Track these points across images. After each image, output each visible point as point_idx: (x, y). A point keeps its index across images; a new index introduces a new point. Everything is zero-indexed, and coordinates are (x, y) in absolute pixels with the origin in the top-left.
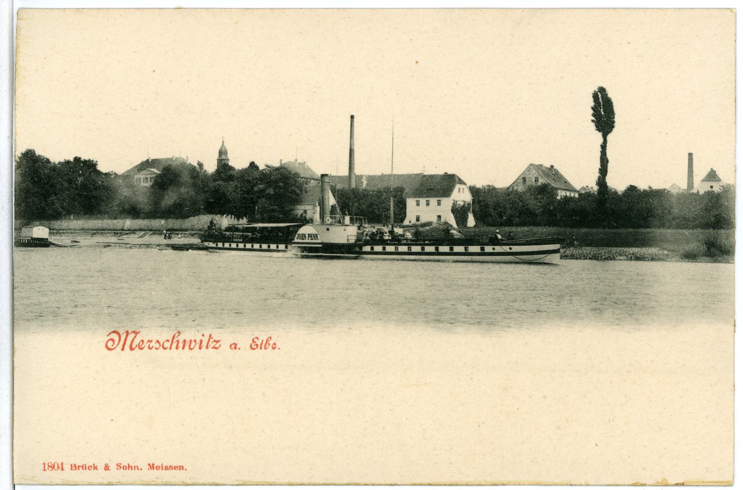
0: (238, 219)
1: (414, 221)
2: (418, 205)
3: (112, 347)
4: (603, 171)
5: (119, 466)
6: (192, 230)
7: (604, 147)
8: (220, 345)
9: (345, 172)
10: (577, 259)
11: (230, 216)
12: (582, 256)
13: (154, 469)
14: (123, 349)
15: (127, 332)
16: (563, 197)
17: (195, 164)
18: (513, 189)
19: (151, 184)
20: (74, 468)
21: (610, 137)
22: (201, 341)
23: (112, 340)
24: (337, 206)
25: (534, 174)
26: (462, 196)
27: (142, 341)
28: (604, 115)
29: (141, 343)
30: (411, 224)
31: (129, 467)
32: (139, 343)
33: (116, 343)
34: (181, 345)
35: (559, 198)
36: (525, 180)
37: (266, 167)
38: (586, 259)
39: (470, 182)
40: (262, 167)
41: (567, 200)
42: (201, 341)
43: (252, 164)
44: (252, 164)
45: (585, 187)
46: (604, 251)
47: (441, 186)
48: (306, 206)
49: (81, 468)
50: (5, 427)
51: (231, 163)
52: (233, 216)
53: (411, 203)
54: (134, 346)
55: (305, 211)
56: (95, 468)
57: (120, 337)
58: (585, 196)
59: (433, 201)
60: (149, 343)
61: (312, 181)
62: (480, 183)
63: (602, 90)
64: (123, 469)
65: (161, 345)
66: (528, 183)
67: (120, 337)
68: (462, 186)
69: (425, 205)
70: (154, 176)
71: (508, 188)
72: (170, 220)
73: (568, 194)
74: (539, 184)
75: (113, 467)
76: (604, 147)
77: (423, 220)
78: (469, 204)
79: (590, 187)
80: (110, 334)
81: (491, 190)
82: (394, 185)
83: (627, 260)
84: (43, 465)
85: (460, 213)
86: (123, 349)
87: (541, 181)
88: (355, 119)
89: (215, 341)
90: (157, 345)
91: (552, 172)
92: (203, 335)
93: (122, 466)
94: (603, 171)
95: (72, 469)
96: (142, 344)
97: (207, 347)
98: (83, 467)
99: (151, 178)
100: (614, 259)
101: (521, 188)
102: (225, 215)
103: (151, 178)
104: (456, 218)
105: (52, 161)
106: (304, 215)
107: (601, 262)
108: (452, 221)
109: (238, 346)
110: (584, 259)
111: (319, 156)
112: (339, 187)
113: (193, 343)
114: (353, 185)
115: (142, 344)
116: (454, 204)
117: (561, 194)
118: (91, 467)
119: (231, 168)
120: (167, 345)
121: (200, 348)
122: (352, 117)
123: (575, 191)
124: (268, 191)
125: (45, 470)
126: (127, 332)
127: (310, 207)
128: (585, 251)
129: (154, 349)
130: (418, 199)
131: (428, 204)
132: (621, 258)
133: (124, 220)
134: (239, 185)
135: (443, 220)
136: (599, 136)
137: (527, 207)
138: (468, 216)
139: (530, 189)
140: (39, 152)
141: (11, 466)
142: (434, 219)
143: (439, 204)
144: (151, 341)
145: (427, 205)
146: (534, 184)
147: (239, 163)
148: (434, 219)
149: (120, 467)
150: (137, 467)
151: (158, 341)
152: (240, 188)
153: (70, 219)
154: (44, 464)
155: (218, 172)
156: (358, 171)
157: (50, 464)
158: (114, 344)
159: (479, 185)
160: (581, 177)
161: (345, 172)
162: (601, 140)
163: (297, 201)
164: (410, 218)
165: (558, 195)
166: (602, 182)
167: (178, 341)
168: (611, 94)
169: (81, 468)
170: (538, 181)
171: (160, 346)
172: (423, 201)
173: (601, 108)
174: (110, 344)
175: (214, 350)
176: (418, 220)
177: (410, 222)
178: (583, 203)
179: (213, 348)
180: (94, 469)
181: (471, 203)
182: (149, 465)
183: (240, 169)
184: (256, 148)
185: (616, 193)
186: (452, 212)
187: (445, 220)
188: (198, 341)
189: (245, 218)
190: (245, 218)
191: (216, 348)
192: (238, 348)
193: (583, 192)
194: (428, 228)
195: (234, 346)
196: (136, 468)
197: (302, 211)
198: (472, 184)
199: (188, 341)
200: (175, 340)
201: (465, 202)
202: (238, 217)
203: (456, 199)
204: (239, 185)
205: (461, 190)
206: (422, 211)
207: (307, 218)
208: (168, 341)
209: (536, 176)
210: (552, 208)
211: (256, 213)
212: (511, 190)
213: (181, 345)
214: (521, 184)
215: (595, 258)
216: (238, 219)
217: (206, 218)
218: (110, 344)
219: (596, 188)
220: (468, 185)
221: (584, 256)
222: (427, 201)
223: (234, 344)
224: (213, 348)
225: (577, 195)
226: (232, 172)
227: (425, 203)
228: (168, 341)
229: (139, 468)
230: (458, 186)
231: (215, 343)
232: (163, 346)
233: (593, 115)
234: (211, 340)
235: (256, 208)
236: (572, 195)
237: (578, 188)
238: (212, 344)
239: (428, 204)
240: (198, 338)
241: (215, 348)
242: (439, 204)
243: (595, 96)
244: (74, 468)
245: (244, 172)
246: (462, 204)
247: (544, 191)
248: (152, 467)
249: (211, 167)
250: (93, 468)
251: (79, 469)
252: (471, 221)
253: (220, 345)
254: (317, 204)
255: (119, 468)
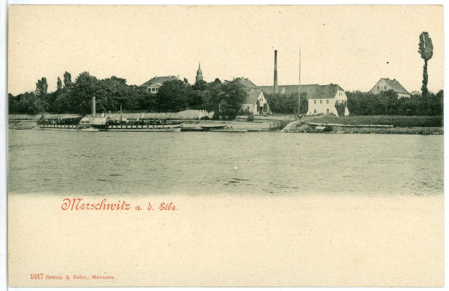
0: (209, 112)
1: (313, 113)
2: (315, 103)
3: (66, 208)
4: (425, 82)
5: (75, 277)
6: (181, 119)
7: (425, 68)
8: (130, 207)
9: (271, 83)
10: (410, 134)
11: (204, 110)
12: (413, 132)
13: (95, 278)
14: (72, 209)
15: (74, 199)
16: (401, 98)
17: (183, 80)
18: (371, 93)
19: (157, 92)
20: (48, 278)
21: (429, 62)
22: (118, 205)
23: (66, 204)
24: (267, 104)
25: (383, 84)
26: (341, 98)
27: (84, 205)
28: (426, 48)
29: (83, 206)
30: (311, 115)
31: (81, 277)
32: (81, 206)
33: (67, 207)
34: (106, 207)
35: (399, 98)
36: (379, 88)
37: (225, 81)
38: (415, 134)
39: (346, 89)
40: (223, 81)
41: (403, 99)
42: (118, 205)
43: (217, 80)
44: (217, 80)
45: (414, 91)
46: (425, 129)
47: (333, 89)
48: (249, 104)
49: (52, 278)
50: (3, 255)
51: (204, 79)
52: (206, 111)
53: (311, 102)
54: (78, 208)
55: (249, 108)
56: (61, 278)
57: (70, 201)
58: (415, 97)
59: (324, 100)
60: (87, 206)
61: (252, 89)
62: (352, 88)
63: (426, 34)
64: (78, 278)
65: (95, 207)
66: (380, 90)
67: (70, 201)
68: (341, 92)
69: (320, 103)
70: (159, 87)
71: (369, 93)
72: (168, 113)
73: (404, 96)
74: (387, 90)
75: (71, 276)
76: (425, 68)
77: (318, 112)
78: (345, 102)
79: (417, 91)
80: (64, 200)
81: (359, 94)
82: (300, 91)
83: (440, 134)
84: (31, 276)
85: (340, 108)
86: (72, 209)
87: (389, 88)
88: (278, 53)
89: (127, 205)
90: (92, 207)
91: (394, 83)
92: (120, 201)
93: (76, 276)
94: (425, 82)
95: (47, 279)
96: (83, 206)
97: (122, 209)
98: (53, 277)
99: (157, 88)
100: (432, 134)
101: (376, 92)
102: (201, 110)
103: (157, 88)
104: (338, 110)
105: (98, 79)
106: (248, 109)
107: (424, 136)
108: (336, 112)
109: (140, 208)
110: (414, 134)
111: (258, 74)
112: (268, 92)
113: (114, 206)
114: (277, 92)
115: (83, 206)
116: (337, 103)
117: (400, 96)
118: (58, 277)
119: (205, 82)
120: (98, 207)
121: (118, 209)
122: (276, 52)
123: (408, 94)
124: (226, 96)
125: (32, 279)
126: (74, 199)
127: (252, 105)
128: (414, 130)
129: (90, 209)
130: (316, 99)
131: (321, 103)
132: (436, 133)
133: (141, 113)
134: (209, 92)
135: (330, 112)
136: (423, 61)
137: (380, 104)
138: (345, 109)
139: (381, 92)
140: (92, 74)
141: (7, 278)
142: (325, 112)
143: (328, 102)
144: (88, 204)
145: (321, 103)
146: (384, 90)
147: (209, 79)
148: (325, 112)
149: (76, 277)
150: (86, 277)
151: (93, 205)
152: (210, 94)
153: (109, 113)
154: (32, 275)
155: (197, 84)
156: (280, 82)
157: (35, 275)
158: (66, 206)
159: (351, 91)
160: (412, 86)
161: (271, 83)
162: (424, 63)
163: (243, 101)
164: (311, 111)
165: (398, 97)
166: (425, 89)
167: (105, 205)
168: (430, 36)
169: (52, 278)
170: (386, 88)
171: (96, 207)
172: (318, 101)
173: (424, 44)
174: (64, 206)
175: (126, 210)
176: (315, 112)
177: (311, 113)
178: (413, 101)
179: (125, 209)
180: (60, 279)
181: (347, 101)
182: (62, 279)
183: (210, 82)
184: (219, 70)
185: (433, 95)
186: (335, 107)
187: (331, 112)
188: (117, 205)
189: (212, 111)
190: (212, 111)
191: (127, 209)
192: (140, 209)
193: (413, 94)
194: (321, 117)
195: (138, 208)
196: (85, 278)
197: (247, 108)
198: (347, 90)
199: (110, 204)
200: (103, 204)
201: (343, 101)
202: (209, 111)
203: (338, 100)
204: (209, 92)
205: (341, 94)
206: (318, 107)
207: (250, 111)
208: (98, 204)
209: (385, 85)
210: (395, 104)
211: (219, 109)
212: (370, 93)
213: (106, 207)
214: (376, 90)
215: (421, 133)
216: (209, 112)
217: (190, 112)
218: (64, 206)
219: (421, 92)
220: (345, 91)
221: (414, 132)
222: (320, 101)
223: (138, 206)
224: (125, 209)
225: (409, 97)
226: (204, 85)
227: (319, 102)
228: (98, 204)
229: (87, 278)
230: (339, 92)
231: (126, 206)
232: (96, 208)
233: (420, 48)
234: (124, 205)
235: (219, 106)
236: (407, 96)
237: (410, 92)
238: (125, 207)
239: (321, 103)
240: (117, 202)
241: (126, 209)
242: (328, 102)
243: (421, 37)
244: (48, 278)
245: (213, 84)
246: (341, 102)
247: (391, 94)
248: (94, 277)
249: (192, 82)
250: (59, 278)
251: (51, 279)
252: (347, 112)
253: (130, 207)
254: (255, 103)
255: (75, 278)
